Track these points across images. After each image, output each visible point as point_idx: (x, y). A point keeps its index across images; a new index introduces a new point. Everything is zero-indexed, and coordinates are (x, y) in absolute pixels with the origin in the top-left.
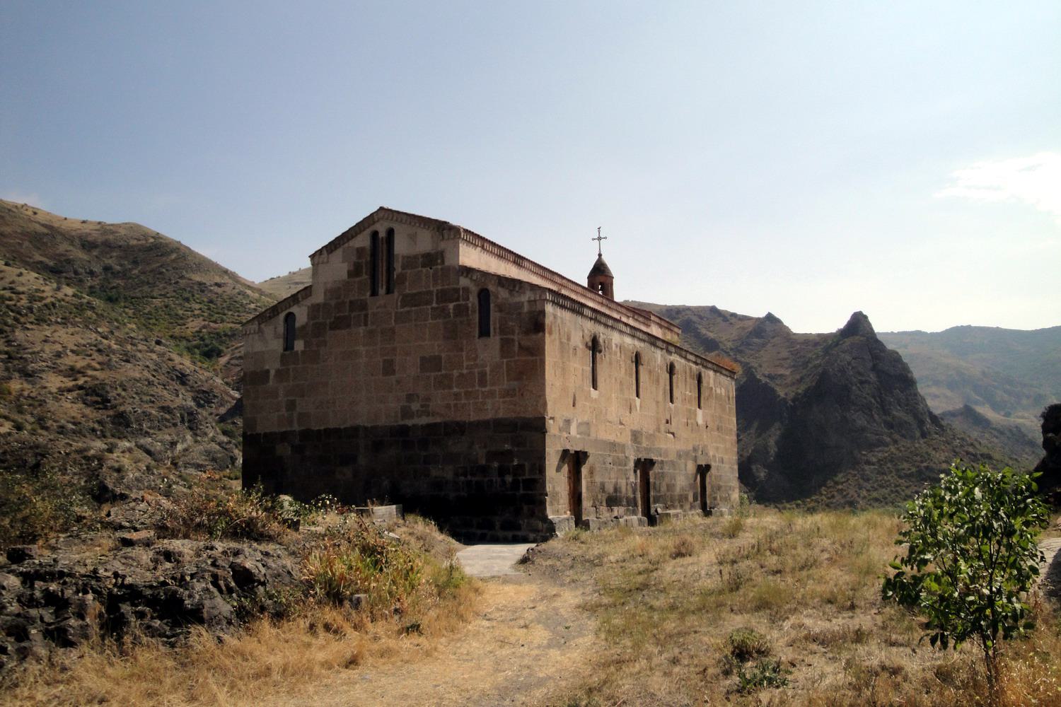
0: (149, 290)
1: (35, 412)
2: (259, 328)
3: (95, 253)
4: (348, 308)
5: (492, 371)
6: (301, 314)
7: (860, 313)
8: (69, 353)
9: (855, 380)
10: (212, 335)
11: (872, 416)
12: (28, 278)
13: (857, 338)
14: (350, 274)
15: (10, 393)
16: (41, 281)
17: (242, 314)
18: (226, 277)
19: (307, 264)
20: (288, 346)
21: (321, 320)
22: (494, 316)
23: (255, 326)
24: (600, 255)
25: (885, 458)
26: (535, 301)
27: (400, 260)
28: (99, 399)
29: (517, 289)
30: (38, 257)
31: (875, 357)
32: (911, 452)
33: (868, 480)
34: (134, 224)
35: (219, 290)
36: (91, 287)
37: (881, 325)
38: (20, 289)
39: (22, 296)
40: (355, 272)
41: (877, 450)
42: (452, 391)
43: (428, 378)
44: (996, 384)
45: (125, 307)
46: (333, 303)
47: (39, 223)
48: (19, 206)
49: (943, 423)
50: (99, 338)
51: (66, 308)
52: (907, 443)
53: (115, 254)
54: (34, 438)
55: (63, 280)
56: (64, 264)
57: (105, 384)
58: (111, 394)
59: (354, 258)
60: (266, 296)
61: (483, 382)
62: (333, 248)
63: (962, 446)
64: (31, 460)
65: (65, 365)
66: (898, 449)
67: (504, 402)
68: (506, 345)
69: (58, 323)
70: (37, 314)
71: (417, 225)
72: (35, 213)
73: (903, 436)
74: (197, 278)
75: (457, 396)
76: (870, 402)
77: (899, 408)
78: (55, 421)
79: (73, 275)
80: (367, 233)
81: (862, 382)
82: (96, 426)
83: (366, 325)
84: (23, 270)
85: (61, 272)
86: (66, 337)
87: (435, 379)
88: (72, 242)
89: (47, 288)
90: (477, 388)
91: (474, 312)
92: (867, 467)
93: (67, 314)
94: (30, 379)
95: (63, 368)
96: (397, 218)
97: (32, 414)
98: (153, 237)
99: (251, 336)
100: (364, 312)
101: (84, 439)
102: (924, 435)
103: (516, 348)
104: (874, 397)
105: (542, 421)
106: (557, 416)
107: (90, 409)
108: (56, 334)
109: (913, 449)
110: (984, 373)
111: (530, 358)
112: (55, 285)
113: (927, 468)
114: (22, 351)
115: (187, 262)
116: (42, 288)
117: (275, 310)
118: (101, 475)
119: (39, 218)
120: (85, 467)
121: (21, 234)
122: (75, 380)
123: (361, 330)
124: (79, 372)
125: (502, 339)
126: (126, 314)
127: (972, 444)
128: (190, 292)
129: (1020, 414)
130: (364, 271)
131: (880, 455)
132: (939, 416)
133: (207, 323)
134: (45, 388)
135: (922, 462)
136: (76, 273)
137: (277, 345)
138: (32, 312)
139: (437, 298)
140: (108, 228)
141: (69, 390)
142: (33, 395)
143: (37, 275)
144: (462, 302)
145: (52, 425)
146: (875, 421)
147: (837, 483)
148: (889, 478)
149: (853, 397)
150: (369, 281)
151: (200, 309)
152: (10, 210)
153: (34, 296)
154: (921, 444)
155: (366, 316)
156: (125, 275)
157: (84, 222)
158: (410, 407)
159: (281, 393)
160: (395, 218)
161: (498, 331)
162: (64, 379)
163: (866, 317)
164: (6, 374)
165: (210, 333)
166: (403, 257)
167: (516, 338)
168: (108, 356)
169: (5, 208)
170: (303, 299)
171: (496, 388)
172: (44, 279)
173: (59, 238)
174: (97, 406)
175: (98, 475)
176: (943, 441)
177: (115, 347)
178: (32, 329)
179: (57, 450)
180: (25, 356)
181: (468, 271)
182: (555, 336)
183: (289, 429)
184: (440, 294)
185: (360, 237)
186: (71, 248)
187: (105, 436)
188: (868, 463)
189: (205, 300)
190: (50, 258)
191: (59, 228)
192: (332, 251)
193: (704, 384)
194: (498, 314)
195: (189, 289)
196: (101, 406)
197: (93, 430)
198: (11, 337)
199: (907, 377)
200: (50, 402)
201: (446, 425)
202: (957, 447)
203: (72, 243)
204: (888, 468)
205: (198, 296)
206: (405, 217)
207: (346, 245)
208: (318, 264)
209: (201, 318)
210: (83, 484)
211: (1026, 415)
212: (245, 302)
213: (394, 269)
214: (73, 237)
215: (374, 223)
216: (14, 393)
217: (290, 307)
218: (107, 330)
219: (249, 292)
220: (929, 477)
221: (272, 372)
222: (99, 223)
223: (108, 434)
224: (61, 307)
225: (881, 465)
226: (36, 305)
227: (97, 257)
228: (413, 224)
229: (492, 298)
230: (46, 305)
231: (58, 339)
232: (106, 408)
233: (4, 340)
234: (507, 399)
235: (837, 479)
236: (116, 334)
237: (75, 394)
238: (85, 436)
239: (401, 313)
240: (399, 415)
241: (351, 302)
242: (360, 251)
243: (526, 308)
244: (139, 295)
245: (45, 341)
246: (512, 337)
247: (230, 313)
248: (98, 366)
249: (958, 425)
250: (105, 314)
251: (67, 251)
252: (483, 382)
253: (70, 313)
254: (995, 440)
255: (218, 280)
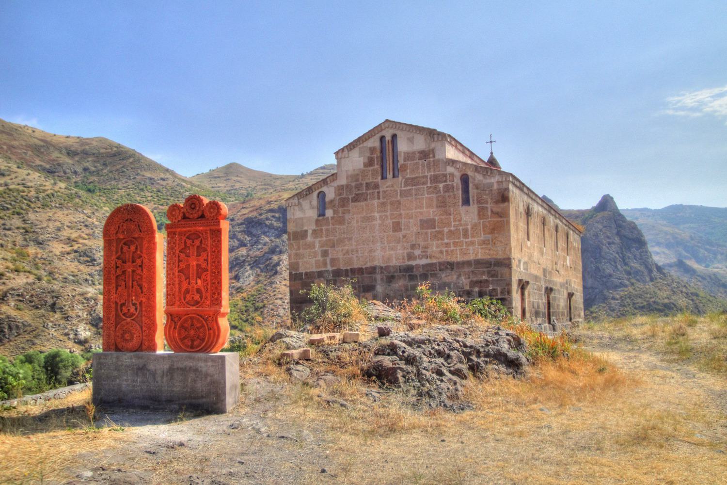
0: (116, 183)
1: (47, 268)
2: (299, 202)
3: (77, 158)
4: (364, 188)
5: (472, 228)
6: (330, 193)
7: (608, 195)
8: (66, 228)
9: (605, 242)
10: (160, 214)
11: (616, 267)
12: (34, 177)
13: (606, 212)
14: (365, 165)
15: (29, 256)
16: (43, 179)
17: (180, 199)
18: (168, 174)
19: (334, 161)
20: (322, 214)
21: (344, 196)
22: (472, 191)
23: (295, 201)
24: (492, 153)
25: (626, 295)
26: (502, 182)
27: (403, 154)
28: (89, 259)
29: (489, 174)
30: (38, 162)
31: (619, 226)
32: (643, 291)
33: (613, 310)
34: (102, 138)
35: (164, 183)
36: (75, 182)
37: (623, 204)
38: (29, 184)
39: (31, 189)
40: (370, 163)
41: (620, 290)
42: (444, 242)
43: (426, 233)
44: (699, 244)
45: (100, 196)
46: (353, 184)
47: (36, 138)
48: (22, 127)
49: (665, 271)
50: (86, 218)
51: (61, 197)
52: (639, 285)
53: (90, 159)
54: (50, 286)
55: (56, 177)
56: (57, 166)
57: (92, 249)
58: (96, 256)
59: (368, 154)
60: (195, 186)
61: (466, 235)
62: (352, 147)
63: (678, 287)
64: (50, 301)
65: (64, 236)
66: (634, 289)
67: (482, 248)
68: (481, 212)
69: (56, 207)
70: (43, 201)
71: (415, 131)
72: (34, 132)
73: (638, 280)
74: (148, 175)
75: (447, 245)
76: (615, 257)
77: (635, 261)
78: (60, 274)
79: (63, 175)
80: (378, 136)
81: (609, 244)
82: (88, 277)
83: (379, 199)
84: (30, 171)
85: (55, 172)
86: (64, 217)
87: (431, 234)
88: (59, 150)
89: (47, 184)
90: (462, 239)
91: (457, 189)
92: (612, 302)
93: (63, 201)
94: (41, 246)
95: (62, 238)
96: (399, 127)
97: (45, 270)
98: (116, 147)
99: (292, 207)
100: (376, 191)
101: (81, 286)
102: (652, 280)
103: (489, 213)
104: (617, 253)
105: (509, 259)
106: (516, 257)
107: (83, 266)
108: (56, 215)
109: (645, 289)
110: (691, 237)
111: (500, 219)
112: (52, 181)
113: (654, 302)
114: (34, 227)
115: (142, 164)
116: (44, 184)
117: (310, 190)
118: (97, 310)
119: (36, 134)
120: (86, 305)
121: (26, 146)
122: (72, 246)
123: (376, 202)
124: (74, 241)
125: (479, 207)
126: (101, 200)
127: (685, 286)
128: (144, 184)
129: (716, 265)
130: (376, 162)
131: (622, 293)
132: (662, 267)
133: (156, 206)
134: (52, 252)
135: (651, 298)
136: (65, 173)
137: (313, 214)
138: (39, 200)
139: (431, 181)
140: (84, 141)
141: (68, 253)
142: (44, 257)
143: (39, 175)
144: (448, 183)
145: (59, 277)
146: (618, 270)
147: (592, 312)
148: (629, 309)
149: (603, 253)
150: (379, 169)
151: (152, 196)
152: (16, 130)
153: (39, 189)
154: (650, 286)
155: (379, 193)
156: (98, 173)
157: (68, 137)
158: (413, 253)
159: (317, 245)
160: (397, 127)
161: (475, 201)
162: (64, 246)
163: (612, 198)
164: (25, 243)
165: (159, 213)
166: (404, 153)
167: (489, 206)
168: (92, 229)
169: (13, 128)
170: (331, 182)
171: (476, 239)
172: (45, 178)
173: (52, 149)
174: (88, 264)
175: (95, 310)
176: (665, 284)
177: (97, 223)
178: (40, 212)
179: (66, 294)
180: (36, 230)
181: (453, 162)
182: (514, 205)
183: (323, 269)
184: (432, 178)
185: (372, 140)
186: (61, 156)
187: (94, 284)
188: (614, 298)
189: (155, 190)
190: (48, 162)
191: (51, 141)
192: (351, 149)
193: (569, 239)
194: (475, 191)
195: (143, 182)
196: (90, 264)
197: (86, 280)
198: (26, 218)
199: (641, 239)
200: (56, 260)
201: (440, 264)
202: (674, 288)
203: (61, 152)
204: (627, 302)
205: (149, 187)
206: (405, 126)
207: (361, 145)
208: (341, 159)
209: (153, 203)
210: (85, 316)
211: (720, 266)
212: (182, 191)
213: (398, 161)
214: (61, 147)
215: (382, 130)
216: (31, 256)
217: (321, 187)
218: (90, 211)
219: (184, 184)
220: (656, 308)
221: (310, 232)
222: (78, 138)
223: (96, 283)
224: (58, 196)
225: (623, 300)
226: (41, 195)
227: (78, 161)
228: (411, 131)
229: (471, 180)
230: (48, 195)
231: (57, 218)
232: (93, 265)
233: (22, 219)
234: (483, 246)
235: (592, 310)
236: (96, 214)
237: (72, 255)
238: (81, 284)
239: (405, 190)
240: (406, 258)
241: (367, 183)
242: (372, 150)
243: (495, 187)
244: (109, 187)
245: (49, 220)
246: (486, 206)
247: (172, 199)
248: (86, 237)
249: (674, 273)
250: (88, 201)
251: (58, 158)
252: (466, 235)
253: (65, 200)
254: (699, 283)
255: (162, 176)
